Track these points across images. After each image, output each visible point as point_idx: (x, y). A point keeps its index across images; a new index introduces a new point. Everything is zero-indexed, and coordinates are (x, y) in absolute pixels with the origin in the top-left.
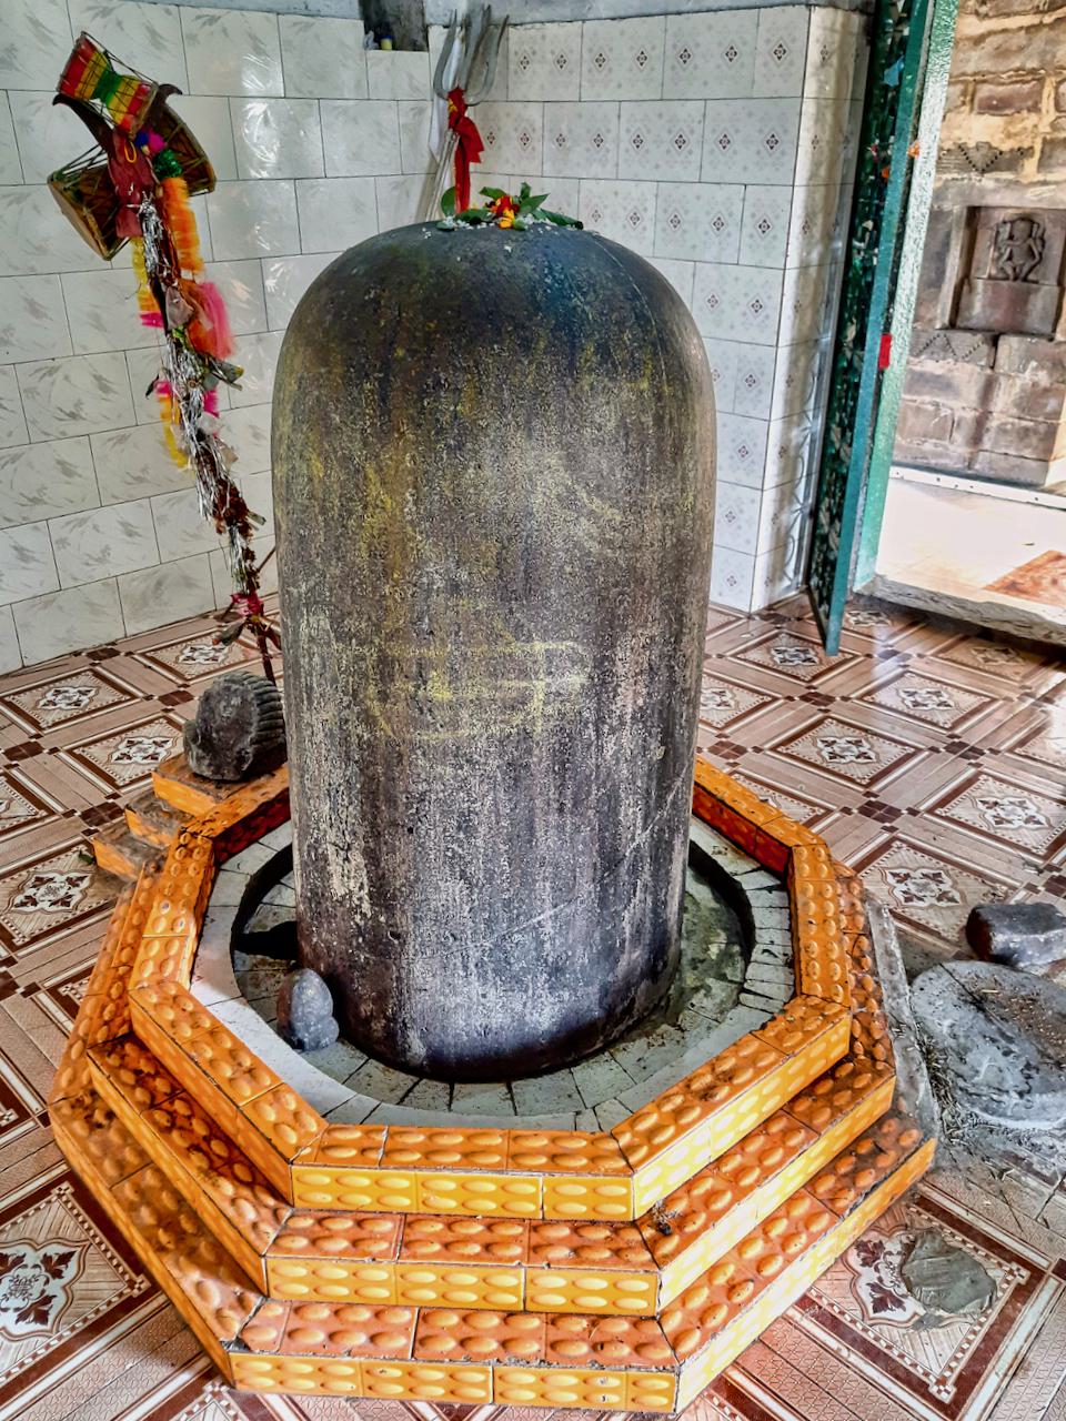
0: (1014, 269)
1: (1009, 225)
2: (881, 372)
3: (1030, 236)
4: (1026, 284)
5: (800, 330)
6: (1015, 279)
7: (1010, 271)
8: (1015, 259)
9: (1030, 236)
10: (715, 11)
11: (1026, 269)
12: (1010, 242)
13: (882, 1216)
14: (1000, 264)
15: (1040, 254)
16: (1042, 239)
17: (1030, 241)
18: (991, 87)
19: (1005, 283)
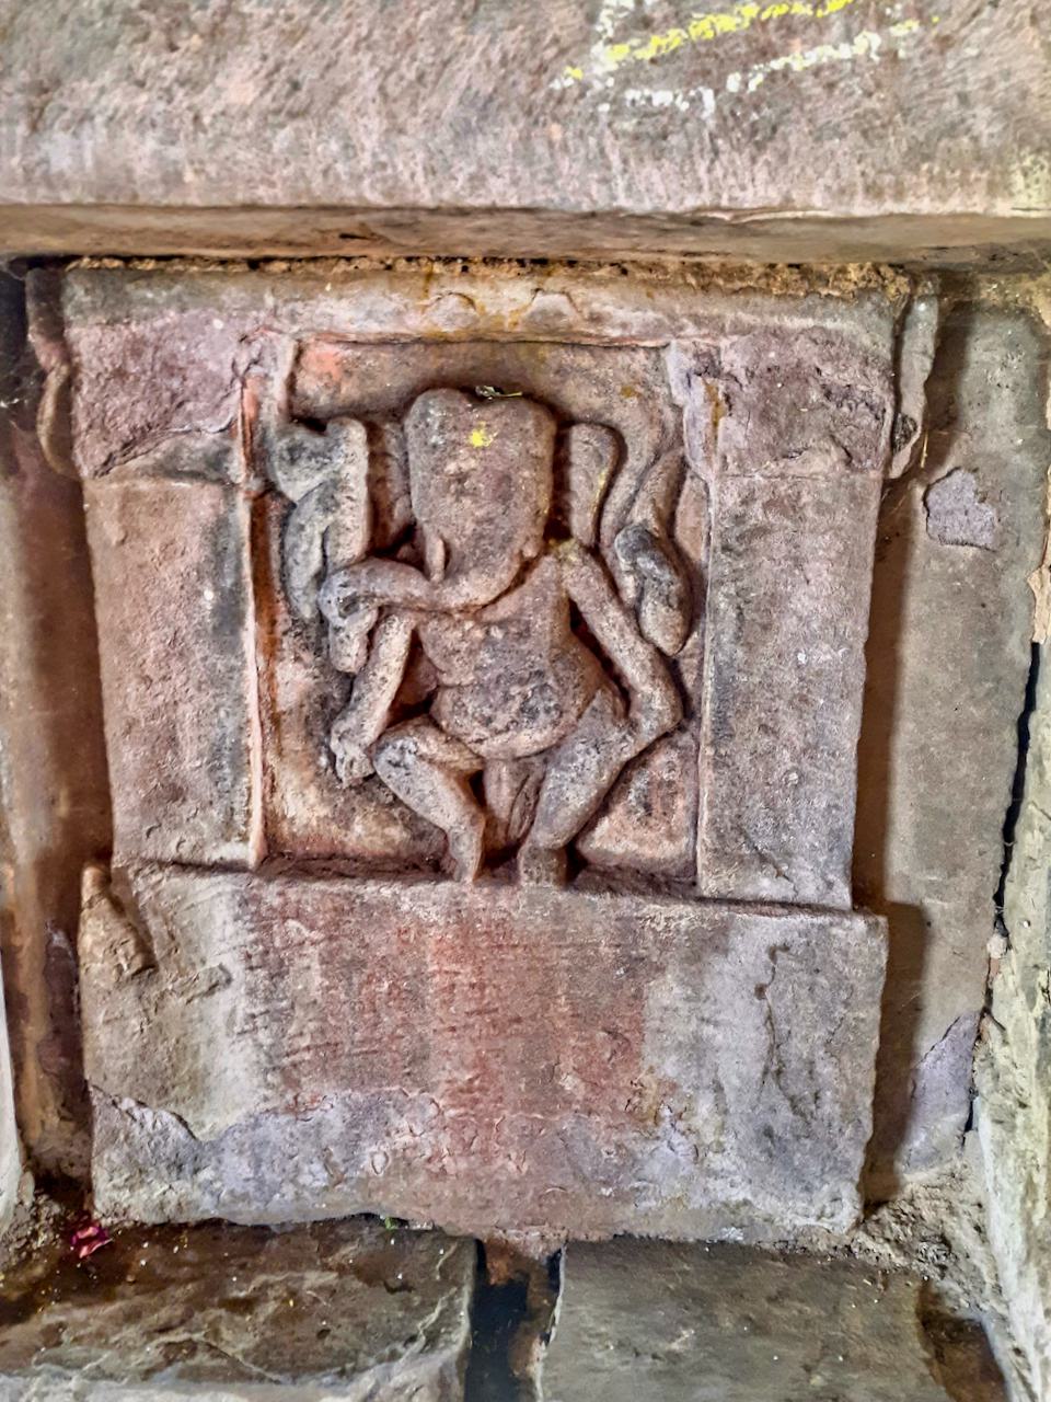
0: (474, 785)
1: (352, 446)
2: (564, 345)
3: (556, 528)
4: (596, 912)
5: (19, 509)
6: (499, 859)
7: (446, 809)
8: (462, 713)
9: (556, 528)
10: (1030, 704)
11: (571, 792)
12: (395, 584)
13: (537, 754)
14: (350, 753)
15: (668, 668)
16: (664, 543)
17: (574, 576)
18: (346, 41)
19: (423, 902)
